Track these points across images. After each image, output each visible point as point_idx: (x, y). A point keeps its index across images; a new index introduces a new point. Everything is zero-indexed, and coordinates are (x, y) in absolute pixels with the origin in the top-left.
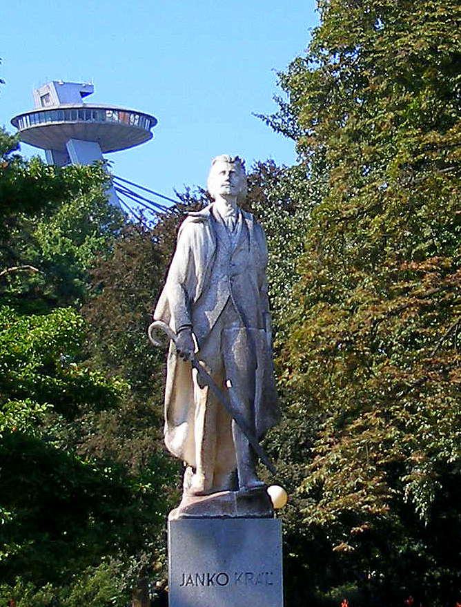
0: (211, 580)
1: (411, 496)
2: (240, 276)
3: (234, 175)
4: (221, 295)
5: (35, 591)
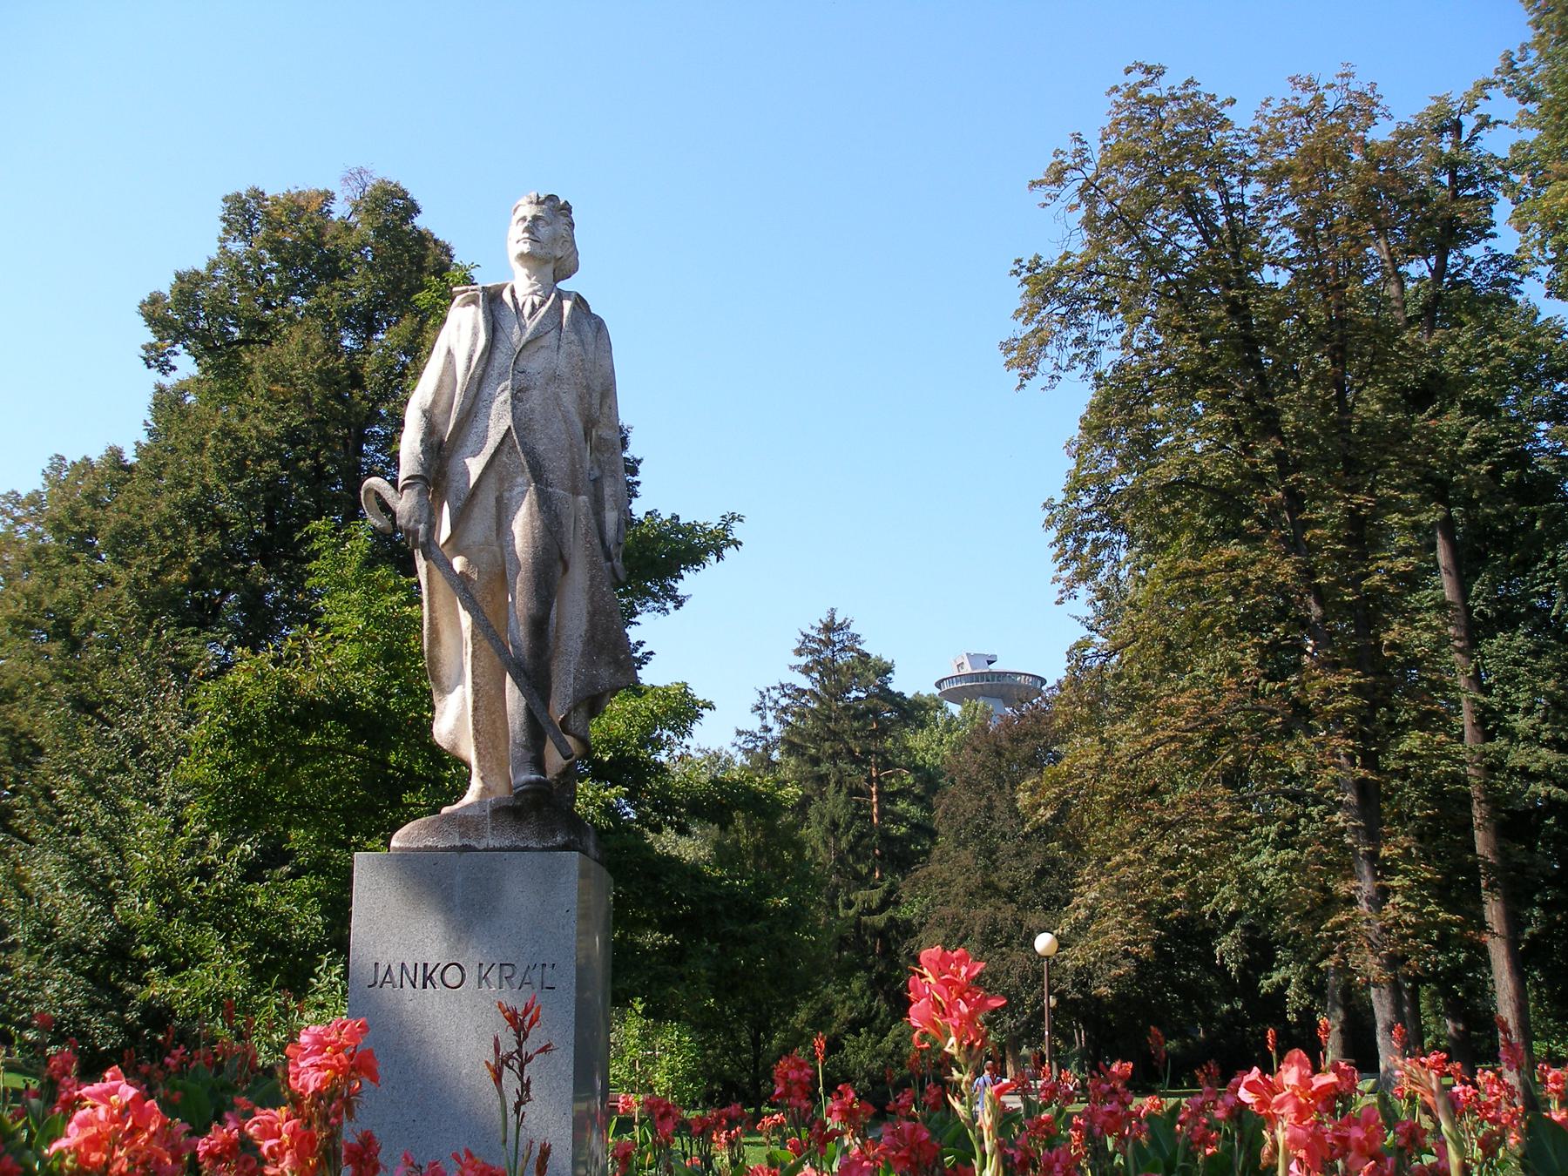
0: (430, 978)
1: (1222, 958)
2: (535, 393)
3: (541, 223)
4: (498, 421)
5: (879, 1042)
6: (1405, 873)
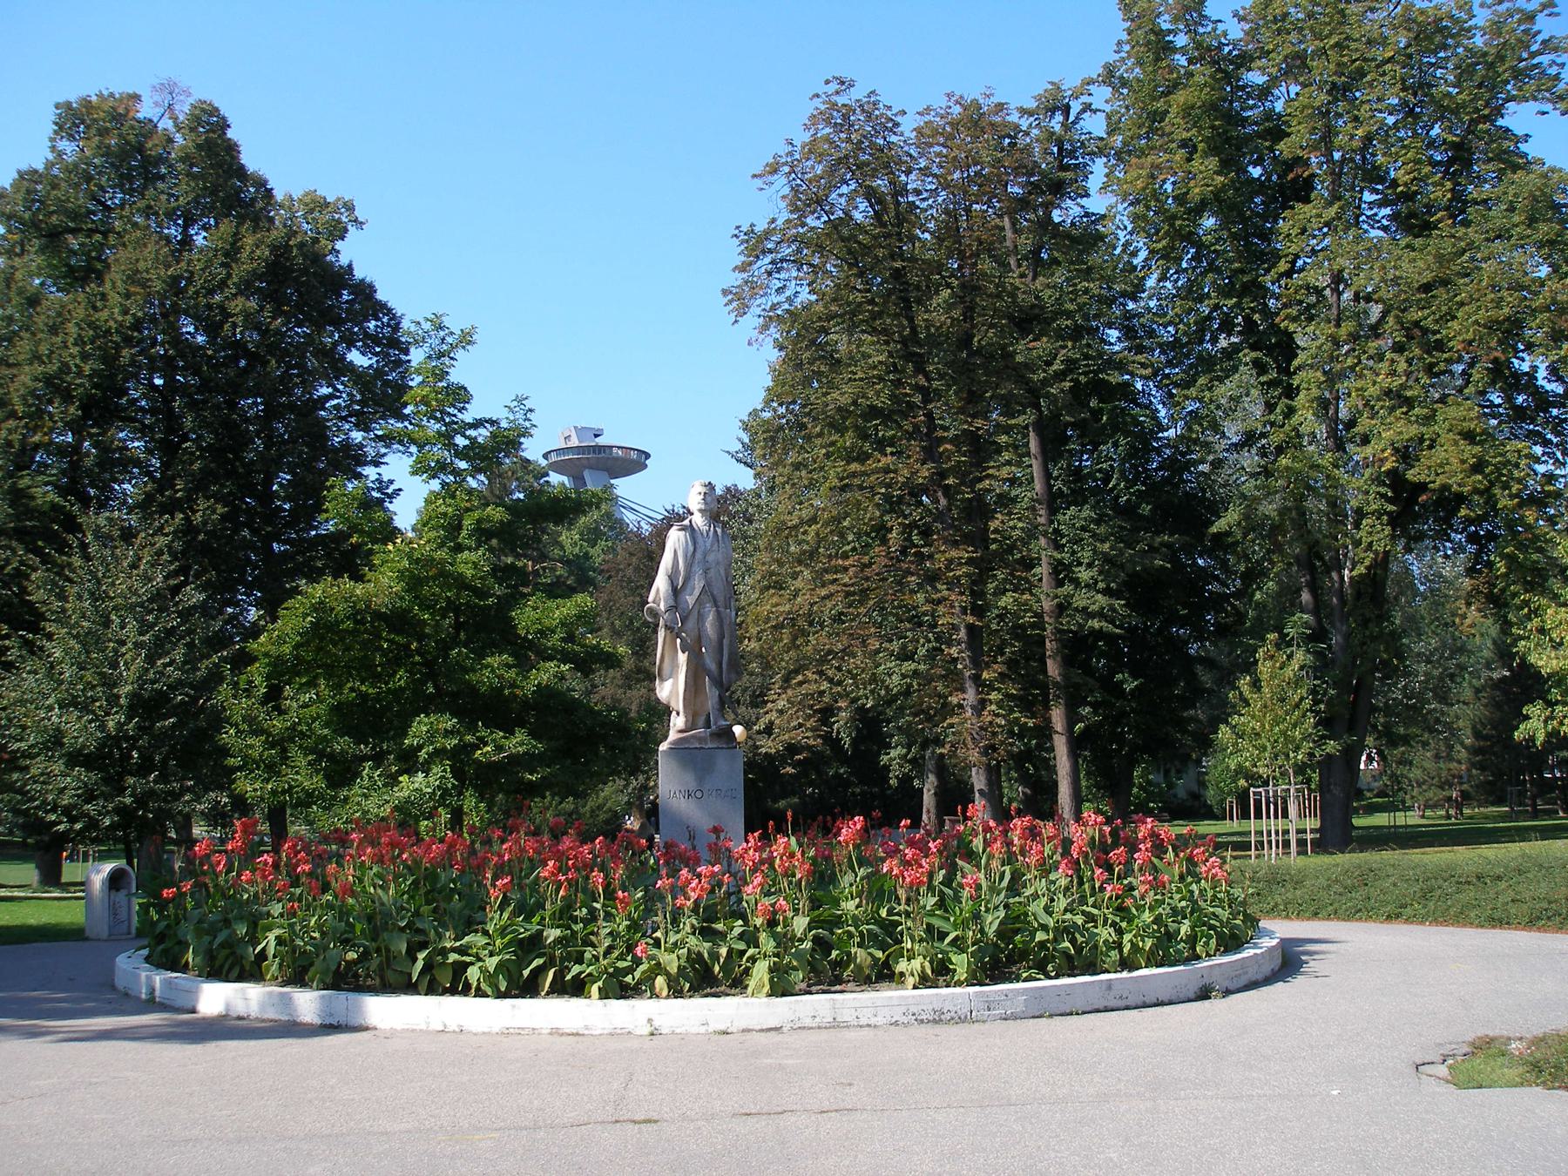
6: (999, 690)
